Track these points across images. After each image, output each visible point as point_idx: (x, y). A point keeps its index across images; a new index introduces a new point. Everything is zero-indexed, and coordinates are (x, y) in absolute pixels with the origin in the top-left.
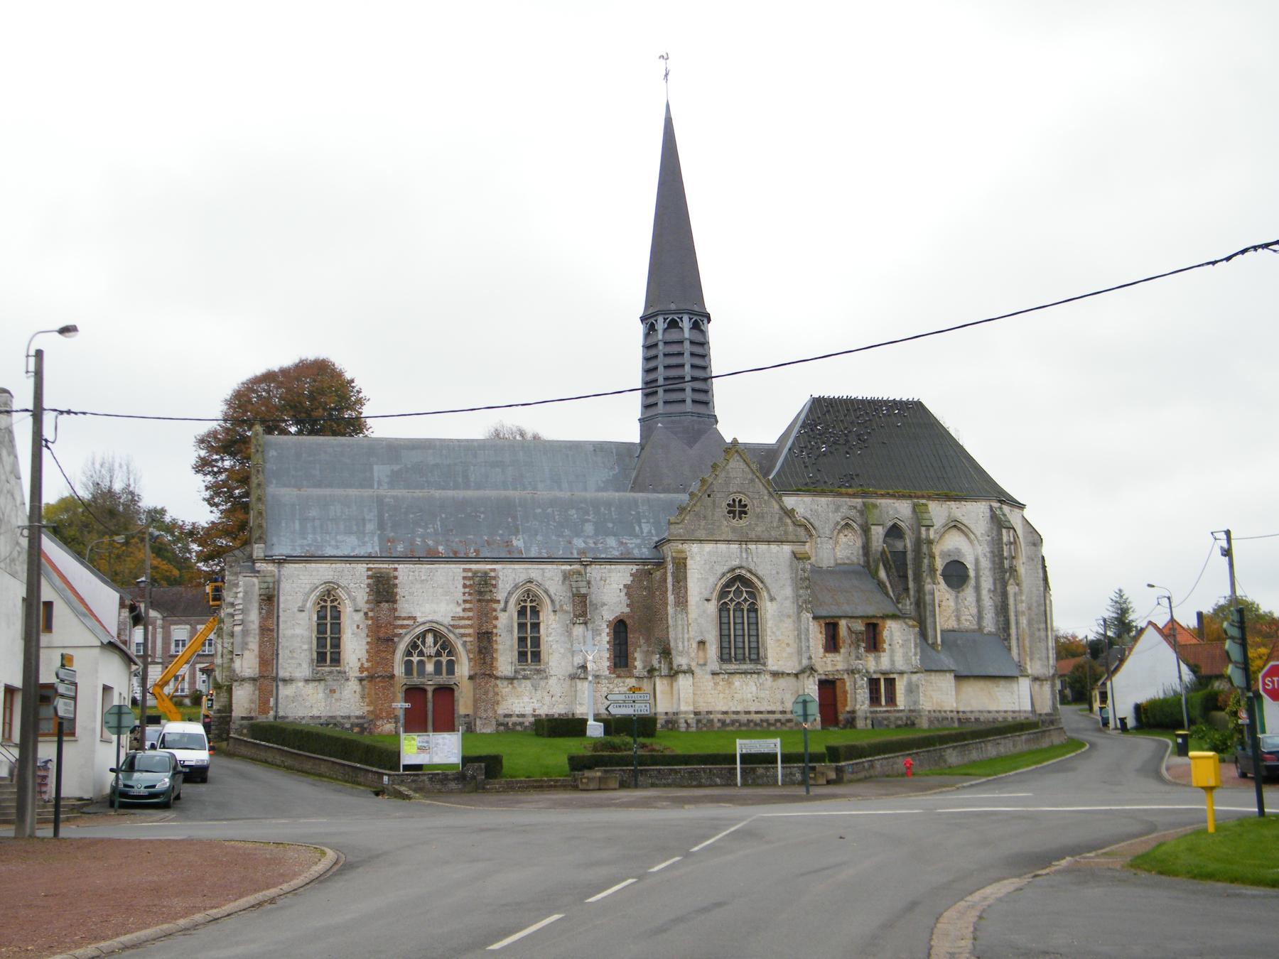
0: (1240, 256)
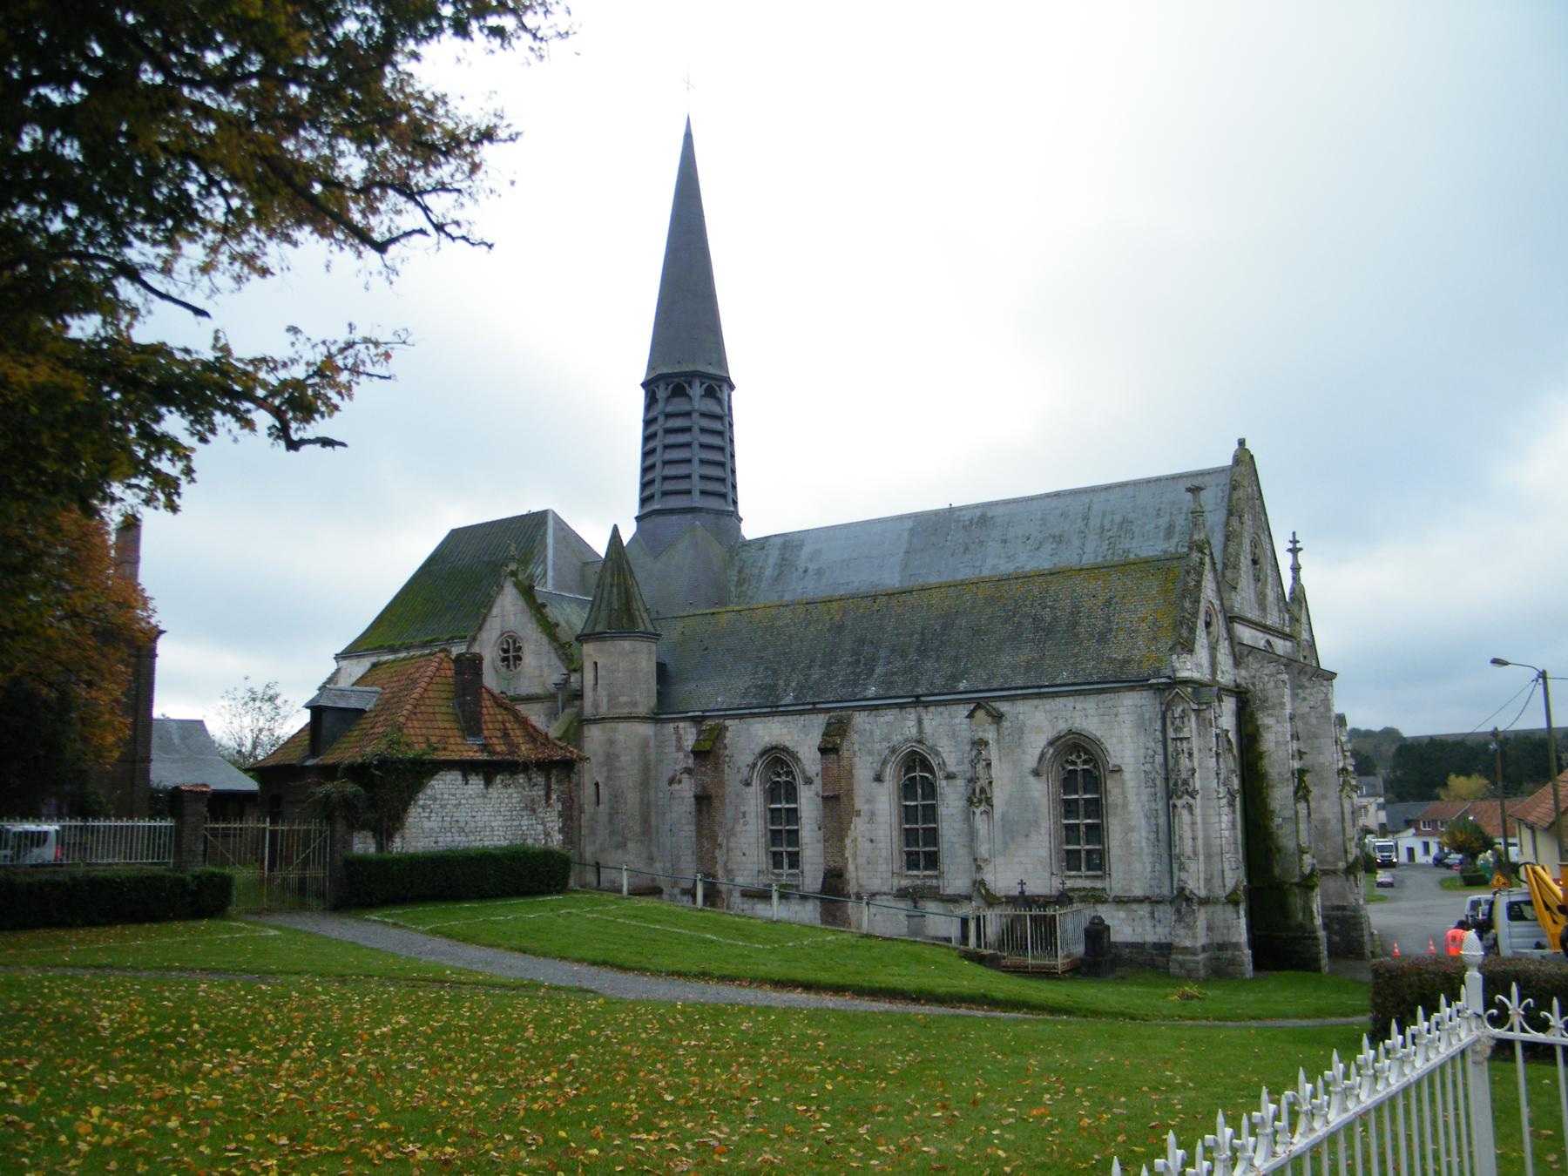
0: (190, 313)
